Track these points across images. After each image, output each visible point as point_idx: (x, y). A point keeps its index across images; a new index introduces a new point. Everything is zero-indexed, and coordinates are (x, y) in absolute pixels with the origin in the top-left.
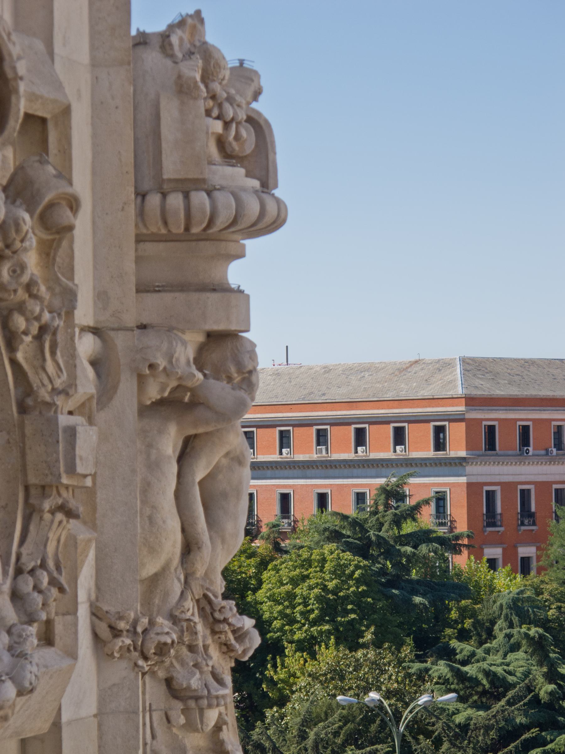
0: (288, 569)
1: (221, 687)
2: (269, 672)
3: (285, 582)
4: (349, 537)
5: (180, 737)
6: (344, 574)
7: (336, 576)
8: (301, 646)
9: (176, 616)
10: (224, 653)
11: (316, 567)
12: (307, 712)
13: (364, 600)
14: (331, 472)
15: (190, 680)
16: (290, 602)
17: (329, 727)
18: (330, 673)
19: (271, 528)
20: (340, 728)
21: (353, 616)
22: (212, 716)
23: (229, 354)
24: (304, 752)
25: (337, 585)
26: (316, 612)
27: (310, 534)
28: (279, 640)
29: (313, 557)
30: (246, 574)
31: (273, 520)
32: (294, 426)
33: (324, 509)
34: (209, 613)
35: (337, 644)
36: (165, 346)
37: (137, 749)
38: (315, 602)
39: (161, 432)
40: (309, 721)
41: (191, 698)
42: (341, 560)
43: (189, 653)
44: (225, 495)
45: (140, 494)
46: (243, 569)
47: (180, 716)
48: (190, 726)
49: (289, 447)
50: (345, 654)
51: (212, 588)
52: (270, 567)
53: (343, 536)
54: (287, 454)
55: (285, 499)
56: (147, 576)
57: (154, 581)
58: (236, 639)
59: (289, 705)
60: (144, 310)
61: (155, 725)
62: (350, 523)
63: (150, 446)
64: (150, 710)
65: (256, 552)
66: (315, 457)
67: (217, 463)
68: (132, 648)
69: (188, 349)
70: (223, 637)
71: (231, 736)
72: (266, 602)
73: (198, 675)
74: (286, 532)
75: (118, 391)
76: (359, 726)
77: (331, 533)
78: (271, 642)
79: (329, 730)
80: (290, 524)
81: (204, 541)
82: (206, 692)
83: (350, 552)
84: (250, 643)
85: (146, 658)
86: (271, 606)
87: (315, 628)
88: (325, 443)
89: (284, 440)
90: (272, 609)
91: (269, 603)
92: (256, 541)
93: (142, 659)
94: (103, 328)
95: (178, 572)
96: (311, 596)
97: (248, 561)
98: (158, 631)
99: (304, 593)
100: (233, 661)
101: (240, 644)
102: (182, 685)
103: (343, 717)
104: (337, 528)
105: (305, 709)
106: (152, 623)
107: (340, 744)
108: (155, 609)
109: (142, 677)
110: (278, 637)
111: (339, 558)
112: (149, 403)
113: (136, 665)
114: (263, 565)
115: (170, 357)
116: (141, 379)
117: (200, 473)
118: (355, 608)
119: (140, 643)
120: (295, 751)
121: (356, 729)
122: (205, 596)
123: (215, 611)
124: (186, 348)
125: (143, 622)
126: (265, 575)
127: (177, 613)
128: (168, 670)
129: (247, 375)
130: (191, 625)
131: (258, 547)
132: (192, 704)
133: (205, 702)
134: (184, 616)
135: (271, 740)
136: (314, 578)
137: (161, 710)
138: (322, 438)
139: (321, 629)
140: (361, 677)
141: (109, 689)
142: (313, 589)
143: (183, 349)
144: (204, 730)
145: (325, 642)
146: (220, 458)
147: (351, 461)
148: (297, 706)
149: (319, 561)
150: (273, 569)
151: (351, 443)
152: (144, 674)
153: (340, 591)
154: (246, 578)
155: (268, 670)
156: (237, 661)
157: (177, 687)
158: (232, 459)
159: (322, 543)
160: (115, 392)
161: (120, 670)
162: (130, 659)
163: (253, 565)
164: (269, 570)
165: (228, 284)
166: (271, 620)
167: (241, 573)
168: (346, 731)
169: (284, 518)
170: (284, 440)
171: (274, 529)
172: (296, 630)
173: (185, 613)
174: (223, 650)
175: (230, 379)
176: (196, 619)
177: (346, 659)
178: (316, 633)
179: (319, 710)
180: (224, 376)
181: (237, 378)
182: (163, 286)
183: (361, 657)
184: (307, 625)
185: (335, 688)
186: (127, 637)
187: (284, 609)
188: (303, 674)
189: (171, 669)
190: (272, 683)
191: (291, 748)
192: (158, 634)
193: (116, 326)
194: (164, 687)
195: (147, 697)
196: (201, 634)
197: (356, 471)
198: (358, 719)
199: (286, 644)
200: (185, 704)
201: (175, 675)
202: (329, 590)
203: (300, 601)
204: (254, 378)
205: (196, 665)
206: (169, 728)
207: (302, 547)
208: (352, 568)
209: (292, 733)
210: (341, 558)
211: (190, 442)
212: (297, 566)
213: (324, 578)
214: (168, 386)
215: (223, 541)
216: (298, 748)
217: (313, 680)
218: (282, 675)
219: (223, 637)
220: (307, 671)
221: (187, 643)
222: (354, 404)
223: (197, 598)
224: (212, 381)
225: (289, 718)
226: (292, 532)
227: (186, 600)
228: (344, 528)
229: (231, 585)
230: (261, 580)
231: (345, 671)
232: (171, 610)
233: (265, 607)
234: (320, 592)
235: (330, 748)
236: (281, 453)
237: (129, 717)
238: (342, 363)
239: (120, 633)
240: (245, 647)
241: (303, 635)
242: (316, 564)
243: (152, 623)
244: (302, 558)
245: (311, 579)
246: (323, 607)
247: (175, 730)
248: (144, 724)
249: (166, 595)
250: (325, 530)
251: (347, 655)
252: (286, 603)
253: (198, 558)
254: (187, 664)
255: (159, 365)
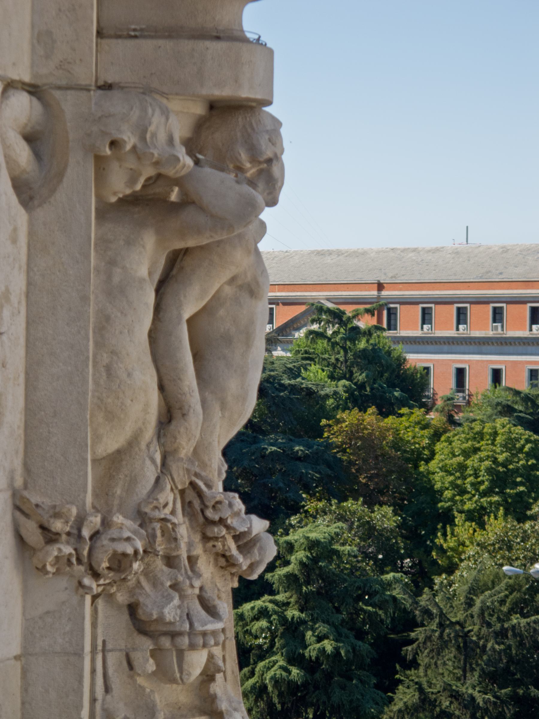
0: (461, 441)
1: (211, 619)
2: (439, 541)
3: (457, 454)
4: (521, 412)
5: (148, 690)
6: (515, 447)
7: (506, 449)
8: (470, 516)
9: (146, 513)
10: (222, 567)
11: (487, 440)
12: (474, 580)
13: (532, 473)
14: (506, 348)
15: (163, 608)
16: (462, 474)
17: (495, 595)
18: (498, 543)
19: (445, 401)
20: (507, 596)
21: (522, 488)
22: (197, 661)
23: (239, 134)
24: (470, 618)
25: (507, 458)
26: (486, 483)
27: (484, 408)
28: (450, 509)
29: (485, 430)
30: (419, 444)
31: (448, 393)
32: (471, 303)
33: (497, 385)
34: (198, 509)
35: (506, 515)
36: (135, 114)
37: (79, 707)
38: (485, 474)
39: (129, 243)
40: (475, 589)
41: (165, 634)
42: (512, 434)
43: (165, 568)
44: (228, 339)
45: (94, 332)
46: (417, 440)
47: (148, 660)
48: (163, 674)
49: (466, 323)
50: (513, 526)
51: (203, 474)
52: (443, 438)
53: (515, 410)
54: (464, 330)
55: (460, 373)
56: (104, 454)
57: (114, 462)
58: (239, 548)
59: (458, 573)
60: (112, 63)
61: (110, 671)
62: (522, 399)
63: (112, 263)
64: (104, 650)
65: (430, 423)
66: (490, 333)
67: (218, 292)
68: (74, 560)
69: (170, 121)
70: (219, 545)
71: (229, 687)
72: (438, 473)
73: (176, 601)
74: (460, 406)
75: (65, 180)
76: (525, 594)
77: (503, 408)
78: (442, 512)
79: (495, 598)
80: (464, 398)
81: (192, 405)
82: (187, 626)
83: (521, 426)
84: (260, 554)
85: (96, 575)
86: (443, 477)
87: (485, 499)
88: (501, 321)
89: (461, 316)
90: (444, 479)
91: (441, 474)
92: (431, 413)
93: (90, 576)
94: (45, 85)
95: (152, 449)
96: (482, 468)
97: (422, 432)
98: (114, 536)
99: (475, 465)
100: (236, 579)
101: (245, 556)
102: (152, 614)
103: (510, 586)
104: (509, 403)
105: (473, 577)
106: (106, 523)
107: (505, 612)
108: (116, 502)
109: (93, 602)
110: (449, 506)
111: (511, 432)
112: (113, 199)
113: (80, 584)
114: (436, 436)
115: (142, 132)
116: (100, 162)
117: (190, 304)
118: (524, 481)
119: (86, 553)
120: (462, 618)
121: (522, 598)
122: (192, 484)
123: (207, 507)
124: (167, 119)
125: (91, 522)
126: (438, 447)
127: (147, 510)
128: (131, 592)
129: (265, 165)
130: (168, 527)
131: (432, 419)
132: (166, 642)
133: (186, 640)
134: (158, 514)
135: (438, 606)
136: (485, 450)
137: (121, 650)
138: (497, 315)
139: (491, 500)
140: (528, 548)
141: (40, 618)
142: (484, 461)
143: (163, 120)
144: (185, 680)
145: (494, 513)
146: (222, 286)
147: (526, 338)
148: (465, 573)
149: (490, 435)
150: (446, 441)
151: (526, 321)
152: (95, 598)
153: (511, 464)
154: (419, 449)
155: (438, 538)
156: (241, 579)
157: (143, 618)
158: (241, 287)
159: (494, 417)
160: (60, 181)
161: (56, 591)
162: (72, 576)
163: (426, 436)
164: (442, 442)
165: (242, 31)
166: (442, 490)
167: (415, 443)
168: (512, 599)
169: (458, 391)
170: (461, 316)
171: (449, 402)
172: (466, 500)
173: (159, 510)
174: (220, 564)
175: (239, 169)
176: (179, 518)
177: (514, 530)
178: (485, 504)
179: (487, 577)
180: (231, 166)
181: (251, 172)
182: (142, 30)
183: (529, 529)
184: (477, 496)
185: (503, 557)
186: (68, 543)
187: (455, 480)
188: (472, 543)
189: (137, 591)
190: (442, 550)
191: (458, 615)
192: (113, 540)
193: (64, 83)
194: (126, 616)
195: (100, 630)
196: (186, 540)
197: (530, 348)
198: (524, 589)
199: (456, 513)
200: (156, 644)
201: (141, 599)
202: (498, 462)
203: (471, 472)
204: (275, 169)
205: (175, 587)
206: (132, 677)
207: (475, 420)
208: (522, 442)
209: (460, 600)
210: (513, 432)
211: (179, 260)
212: (469, 439)
213: (494, 451)
214: (140, 174)
215: (223, 406)
216: (465, 615)
217: (481, 550)
218: (451, 543)
219: (219, 545)
220: (476, 541)
221: (161, 553)
222: (530, 283)
223: (180, 487)
224: (207, 170)
225: (457, 585)
226: (466, 405)
227: (162, 490)
228: (516, 403)
229: (405, 455)
230: (434, 450)
231: (513, 541)
232: (139, 505)
233: (437, 477)
234: (491, 465)
235: (496, 615)
236: (458, 329)
237: (68, 660)
238: (520, 244)
239: (58, 536)
240: (253, 560)
241: (473, 506)
242: (488, 437)
243: (106, 523)
244: (475, 431)
245: (482, 451)
246: (493, 479)
247: (140, 681)
248: (93, 671)
249: (133, 482)
250: (498, 404)
251: (515, 526)
252: (458, 474)
253: (182, 430)
254: (162, 584)
255: (125, 142)
